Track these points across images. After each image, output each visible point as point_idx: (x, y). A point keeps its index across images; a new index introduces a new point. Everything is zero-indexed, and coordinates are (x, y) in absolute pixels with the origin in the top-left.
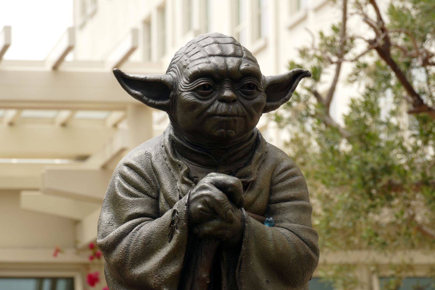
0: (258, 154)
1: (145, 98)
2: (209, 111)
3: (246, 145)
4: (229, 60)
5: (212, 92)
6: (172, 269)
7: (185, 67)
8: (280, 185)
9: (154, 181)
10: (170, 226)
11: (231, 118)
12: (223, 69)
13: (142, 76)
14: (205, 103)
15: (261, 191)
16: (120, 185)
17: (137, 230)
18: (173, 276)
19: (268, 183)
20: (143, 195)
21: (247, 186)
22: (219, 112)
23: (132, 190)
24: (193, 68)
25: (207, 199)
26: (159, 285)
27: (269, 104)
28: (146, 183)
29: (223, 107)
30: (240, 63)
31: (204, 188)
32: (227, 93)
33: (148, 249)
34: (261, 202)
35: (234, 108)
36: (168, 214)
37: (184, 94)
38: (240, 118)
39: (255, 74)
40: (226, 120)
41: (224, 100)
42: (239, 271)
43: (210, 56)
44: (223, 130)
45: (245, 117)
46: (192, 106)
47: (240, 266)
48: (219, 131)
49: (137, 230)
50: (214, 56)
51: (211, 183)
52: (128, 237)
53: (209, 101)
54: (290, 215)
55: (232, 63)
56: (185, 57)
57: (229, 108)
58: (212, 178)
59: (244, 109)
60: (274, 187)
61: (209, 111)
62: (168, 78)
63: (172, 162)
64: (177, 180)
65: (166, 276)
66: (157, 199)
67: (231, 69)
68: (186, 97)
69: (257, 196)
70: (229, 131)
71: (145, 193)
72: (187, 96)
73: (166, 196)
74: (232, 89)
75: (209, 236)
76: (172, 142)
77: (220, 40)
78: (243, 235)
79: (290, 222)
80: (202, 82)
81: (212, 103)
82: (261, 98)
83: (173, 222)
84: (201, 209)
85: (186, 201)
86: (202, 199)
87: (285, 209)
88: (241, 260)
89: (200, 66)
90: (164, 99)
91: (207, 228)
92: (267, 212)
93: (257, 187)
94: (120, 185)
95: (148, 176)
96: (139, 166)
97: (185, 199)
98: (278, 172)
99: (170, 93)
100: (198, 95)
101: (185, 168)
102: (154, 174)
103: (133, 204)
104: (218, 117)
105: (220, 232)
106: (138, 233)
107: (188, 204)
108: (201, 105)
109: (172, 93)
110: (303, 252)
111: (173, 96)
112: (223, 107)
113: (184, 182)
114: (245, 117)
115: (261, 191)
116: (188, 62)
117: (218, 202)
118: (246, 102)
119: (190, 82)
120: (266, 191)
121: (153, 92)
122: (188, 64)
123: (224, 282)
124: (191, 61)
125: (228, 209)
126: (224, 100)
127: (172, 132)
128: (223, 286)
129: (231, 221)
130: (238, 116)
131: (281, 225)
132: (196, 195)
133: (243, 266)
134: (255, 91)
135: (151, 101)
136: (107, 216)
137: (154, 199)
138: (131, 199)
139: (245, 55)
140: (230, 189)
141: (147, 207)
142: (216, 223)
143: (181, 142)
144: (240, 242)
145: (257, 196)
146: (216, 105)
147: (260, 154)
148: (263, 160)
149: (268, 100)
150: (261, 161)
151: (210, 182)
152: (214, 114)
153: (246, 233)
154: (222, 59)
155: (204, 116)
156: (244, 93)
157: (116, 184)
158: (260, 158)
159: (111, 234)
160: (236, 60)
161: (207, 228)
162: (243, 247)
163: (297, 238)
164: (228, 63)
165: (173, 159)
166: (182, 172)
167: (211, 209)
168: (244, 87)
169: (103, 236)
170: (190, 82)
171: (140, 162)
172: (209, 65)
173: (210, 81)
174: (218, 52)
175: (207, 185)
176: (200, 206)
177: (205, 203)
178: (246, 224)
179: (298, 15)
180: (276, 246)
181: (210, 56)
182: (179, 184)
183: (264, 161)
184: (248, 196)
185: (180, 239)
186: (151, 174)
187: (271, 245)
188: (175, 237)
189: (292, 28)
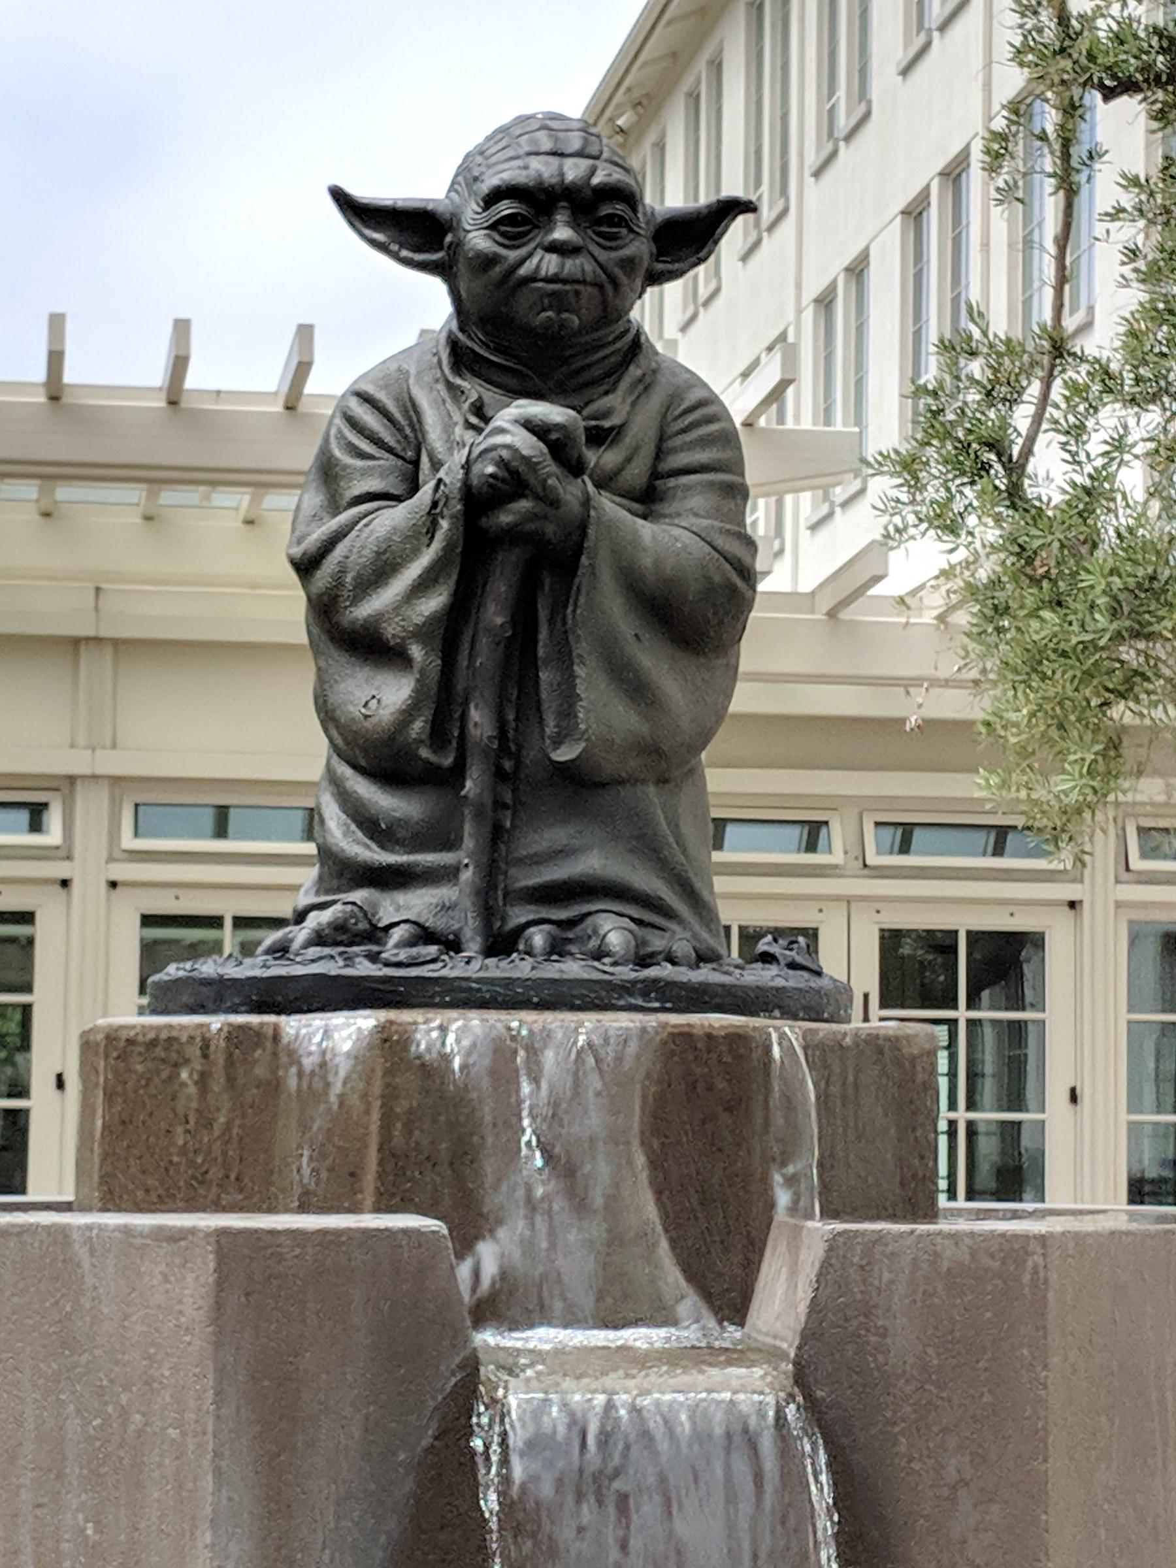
0: (634, 372)
1: (394, 247)
2: (523, 271)
3: (607, 351)
4: (569, 163)
5: (529, 232)
6: (433, 603)
7: (476, 179)
8: (678, 441)
9: (411, 425)
10: (429, 513)
11: (567, 287)
12: (554, 181)
13: (389, 203)
14: (513, 255)
15: (635, 450)
16: (340, 435)
17: (366, 525)
18: (433, 620)
19: (652, 433)
20: (387, 455)
21: (599, 437)
22: (543, 273)
23: (365, 446)
24: (492, 181)
25: (505, 454)
26: (403, 638)
27: (660, 267)
28: (387, 428)
29: (550, 264)
30: (593, 171)
31: (501, 431)
32: (562, 233)
33: (382, 569)
34: (637, 474)
35: (572, 266)
36: (426, 493)
37: (470, 235)
38: (589, 289)
39: (627, 196)
40: (561, 292)
41: (552, 248)
42: (574, 611)
43: (530, 154)
44: (550, 313)
45: (600, 286)
46: (487, 262)
47: (577, 600)
48: (544, 315)
49: (366, 525)
50: (537, 154)
51: (516, 421)
52: (346, 542)
53: (523, 251)
54: (697, 501)
55: (573, 170)
56: (479, 159)
57: (563, 265)
58: (521, 411)
59: (599, 271)
60: (670, 444)
61: (523, 271)
62: (443, 209)
63: (450, 386)
64: (456, 424)
65: (419, 620)
66: (416, 463)
67: (573, 182)
68: (476, 241)
69: (629, 460)
70: (565, 315)
71: (390, 450)
72: (479, 241)
73: (431, 458)
74: (574, 224)
75: (512, 536)
76: (454, 346)
77: (554, 124)
78: (584, 535)
79: (696, 515)
80: (505, 208)
81: (530, 255)
82: (640, 247)
83: (435, 504)
84: (491, 475)
85: (463, 460)
86: (494, 454)
87: (688, 488)
88: (579, 589)
89: (505, 176)
90: (436, 251)
91: (505, 518)
92: (648, 498)
93: (628, 440)
94: (340, 435)
95: (398, 416)
96: (381, 396)
97: (460, 457)
98: (677, 413)
99: (445, 235)
100: (498, 238)
101: (474, 397)
102: (412, 413)
103: (365, 473)
104: (540, 284)
105: (531, 526)
106: (367, 530)
107: (467, 466)
108: (506, 258)
109: (449, 238)
110: (717, 578)
111: (451, 243)
112: (550, 264)
113: (469, 426)
114: (600, 286)
115: (635, 450)
116: (483, 169)
117: (526, 460)
118: (603, 256)
119: (485, 210)
120: (648, 451)
121: (409, 231)
122: (482, 174)
123: (543, 635)
124: (489, 167)
125: (549, 475)
126: (552, 248)
127: (454, 325)
128: (541, 644)
129: (554, 503)
130: (583, 282)
131: (676, 521)
132: (482, 447)
133: (582, 600)
134: (624, 231)
135: (405, 253)
136: (313, 499)
137: (410, 462)
138: (359, 463)
139: (605, 155)
140: (554, 436)
141: (391, 478)
142: (524, 505)
143: (469, 343)
144: (579, 550)
145: (629, 460)
146: (535, 260)
147: (639, 372)
148: (645, 385)
149: (658, 256)
150: (641, 387)
151: (514, 423)
152: (532, 278)
153: (591, 532)
154: (554, 161)
155: (512, 284)
156: (599, 234)
157: (333, 432)
158: (640, 380)
159: (314, 536)
160: (585, 164)
161: (505, 518)
162: (584, 560)
163: (707, 548)
164: (565, 169)
165: (451, 379)
166: (466, 406)
167: (514, 479)
168: (600, 221)
169: (299, 543)
170: (485, 210)
171: (386, 387)
172: (524, 173)
173: (527, 207)
174: (547, 146)
175: (505, 425)
176: (490, 469)
177: (502, 463)
178: (592, 513)
179: (825, 509)
180: (656, 562)
181: (530, 154)
182: (458, 430)
183: (646, 389)
184: (606, 458)
185: (448, 549)
186: (405, 412)
187: (647, 562)
188: (439, 536)
189: (814, 527)
